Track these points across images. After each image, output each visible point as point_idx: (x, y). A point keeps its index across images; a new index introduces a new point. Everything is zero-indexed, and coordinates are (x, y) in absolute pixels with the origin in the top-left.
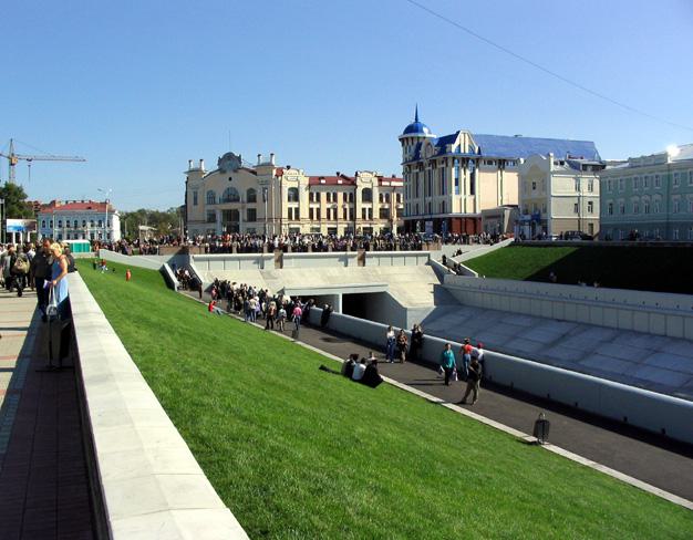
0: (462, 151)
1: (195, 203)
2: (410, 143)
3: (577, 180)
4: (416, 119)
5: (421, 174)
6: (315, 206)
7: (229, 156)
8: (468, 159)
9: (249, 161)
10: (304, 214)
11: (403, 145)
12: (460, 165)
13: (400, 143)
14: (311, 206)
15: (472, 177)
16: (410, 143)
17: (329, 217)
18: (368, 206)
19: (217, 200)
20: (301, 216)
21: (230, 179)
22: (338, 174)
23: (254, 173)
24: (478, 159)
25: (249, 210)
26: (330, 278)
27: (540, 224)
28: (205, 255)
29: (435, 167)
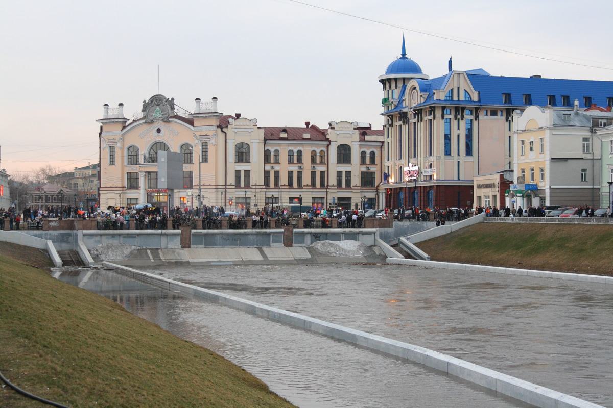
0: (455, 98)
1: (112, 162)
2: (393, 85)
3: (200, 203)
4: (404, 54)
5: (405, 129)
6: (320, 168)
7: (157, 100)
8: (463, 109)
9: (185, 107)
10: (257, 178)
11: (385, 88)
12: (452, 116)
13: (381, 85)
14: (268, 168)
15: (194, 186)
16: (393, 85)
17: (290, 184)
18: (344, 168)
19: (141, 160)
20: (252, 182)
21: (159, 131)
22: (307, 124)
23: (190, 122)
24: (477, 109)
25: (248, 161)
26: (272, 281)
27: (536, 196)
28: (254, 230)
29: (420, 119)
